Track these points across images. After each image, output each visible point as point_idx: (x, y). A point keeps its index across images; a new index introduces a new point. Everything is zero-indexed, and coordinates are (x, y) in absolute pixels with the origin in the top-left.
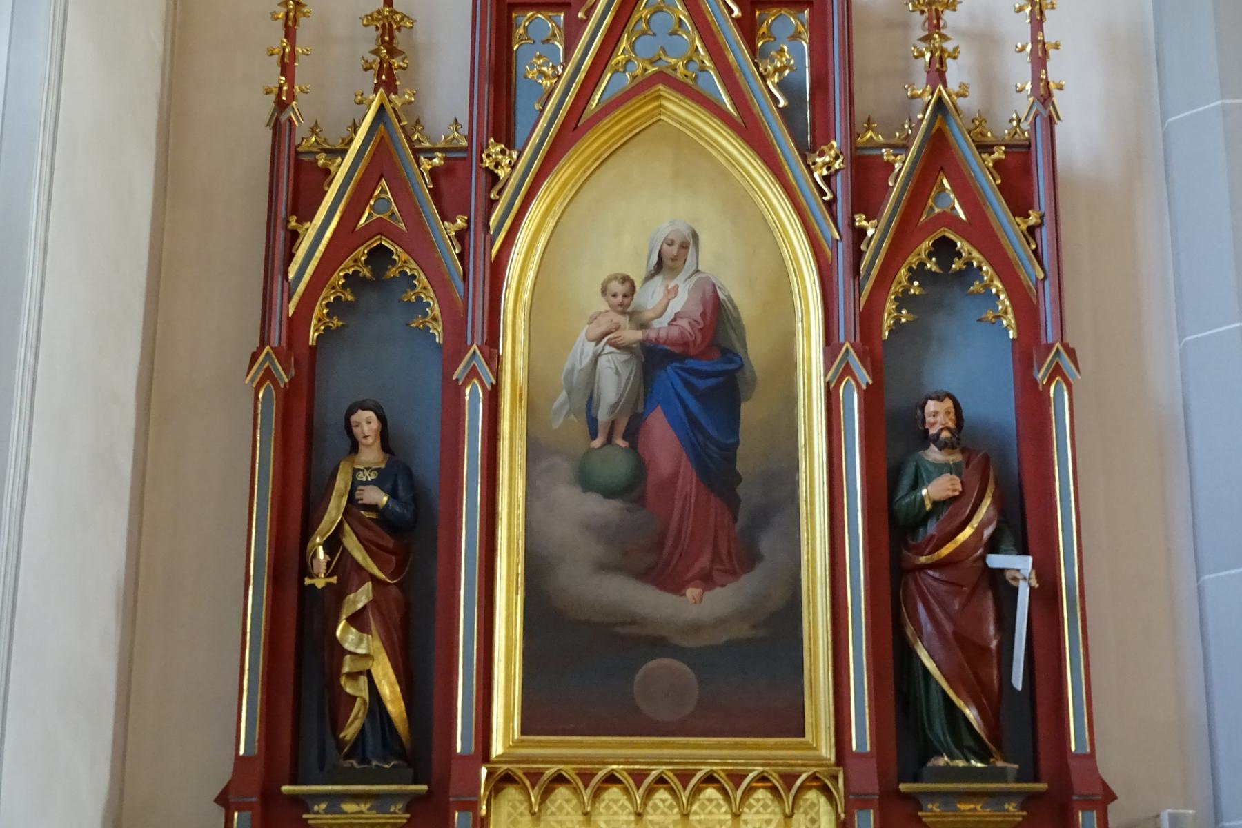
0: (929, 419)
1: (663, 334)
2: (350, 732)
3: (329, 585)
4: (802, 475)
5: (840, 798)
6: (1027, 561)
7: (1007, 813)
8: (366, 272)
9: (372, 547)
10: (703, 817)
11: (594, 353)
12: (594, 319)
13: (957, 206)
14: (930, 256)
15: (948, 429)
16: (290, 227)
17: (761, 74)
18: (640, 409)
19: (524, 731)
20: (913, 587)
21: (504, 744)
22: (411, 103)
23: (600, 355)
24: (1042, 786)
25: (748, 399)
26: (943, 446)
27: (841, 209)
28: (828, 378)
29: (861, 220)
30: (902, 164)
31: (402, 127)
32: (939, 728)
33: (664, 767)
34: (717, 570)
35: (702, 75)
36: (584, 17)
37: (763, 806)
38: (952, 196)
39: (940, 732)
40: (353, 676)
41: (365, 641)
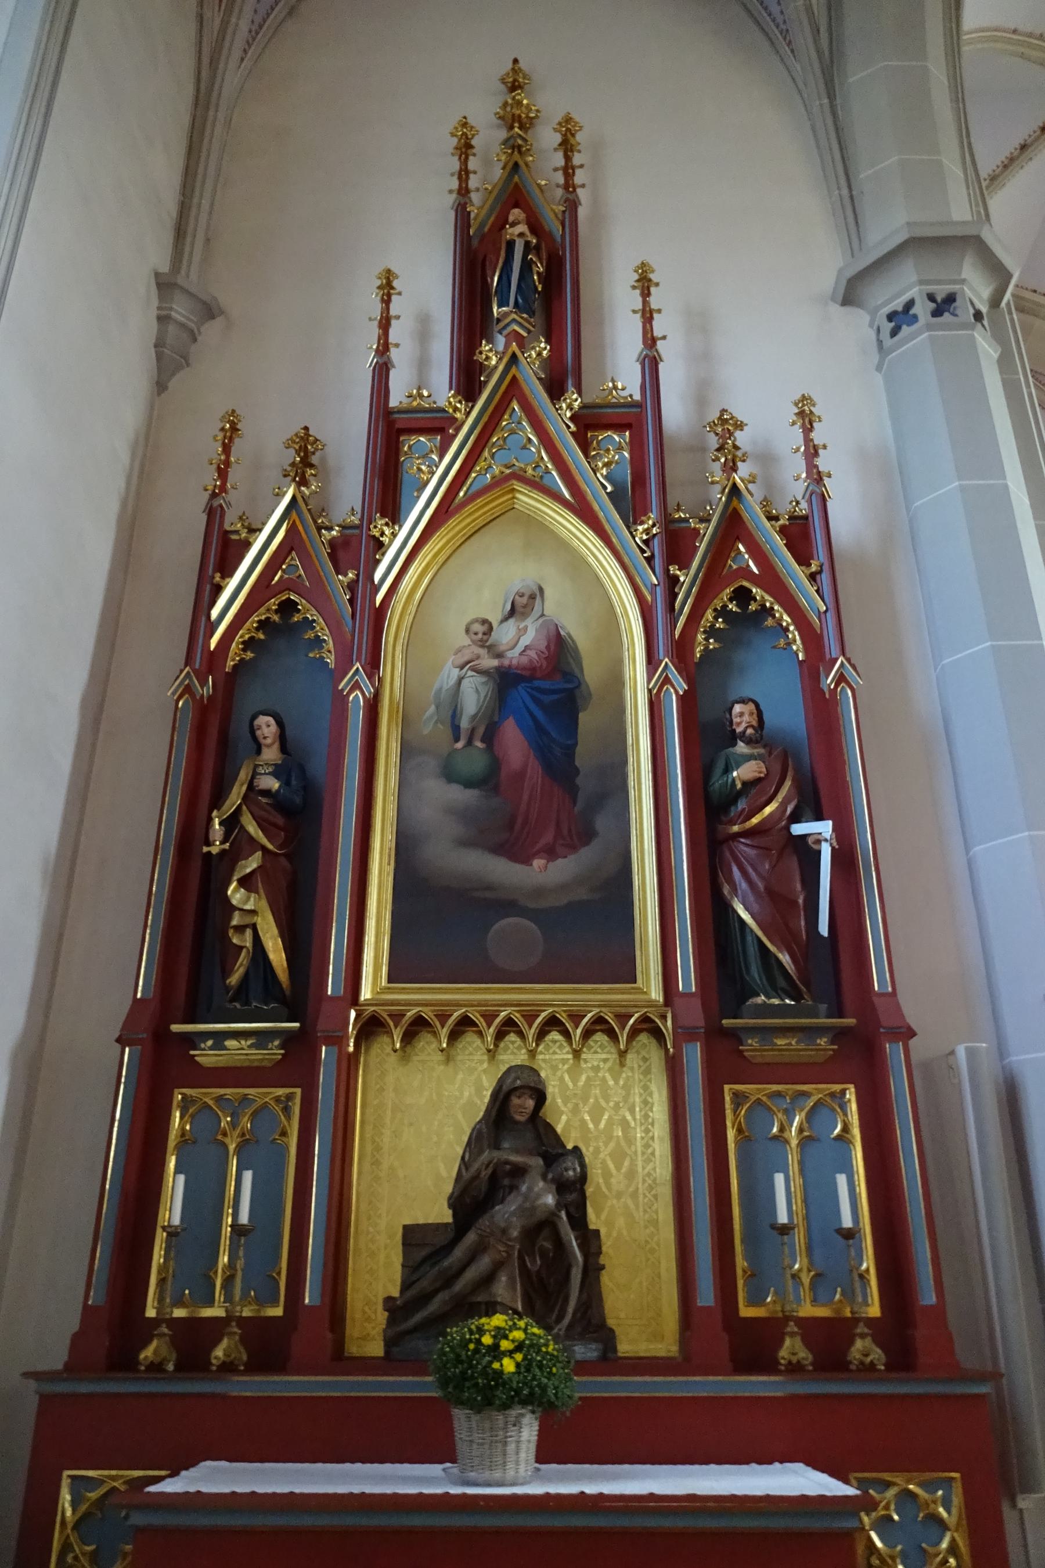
0: (736, 720)
1: (515, 662)
2: (234, 979)
3: (224, 851)
4: (630, 768)
5: (669, 1034)
6: (828, 825)
7: (817, 1047)
8: (276, 618)
9: (264, 824)
10: (547, 1057)
11: (458, 676)
12: (459, 651)
13: (751, 563)
14: (731, 600)
15: (752, 726)
16: (215, 581)
17: (592, 469)
18: (496, 719)
19: (390, 980)
20: (728, 854)
21: (372, 991)
22: (317, 492)
23: (463, 678)
24: (851, 1021)
25: (585, 710)
26: (749, 742)
27: (658, 562)
28: (651, 686)
29: (673, 570)
30: (708, 531)
31: (309, 510)
32: (755, 972)
33: (513, 1008)
34: (563, 845)
35: (547, 476)
36: (454, 433)
37: (600, 1047)
38: (746, 556)
39: (756, 976)
40: (240, 929)
41: (252, 899)
